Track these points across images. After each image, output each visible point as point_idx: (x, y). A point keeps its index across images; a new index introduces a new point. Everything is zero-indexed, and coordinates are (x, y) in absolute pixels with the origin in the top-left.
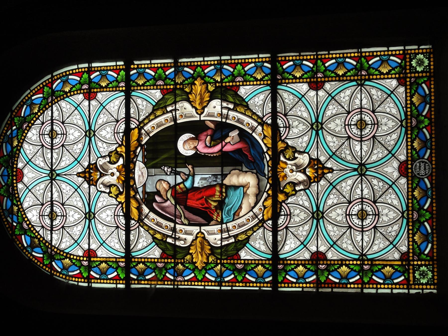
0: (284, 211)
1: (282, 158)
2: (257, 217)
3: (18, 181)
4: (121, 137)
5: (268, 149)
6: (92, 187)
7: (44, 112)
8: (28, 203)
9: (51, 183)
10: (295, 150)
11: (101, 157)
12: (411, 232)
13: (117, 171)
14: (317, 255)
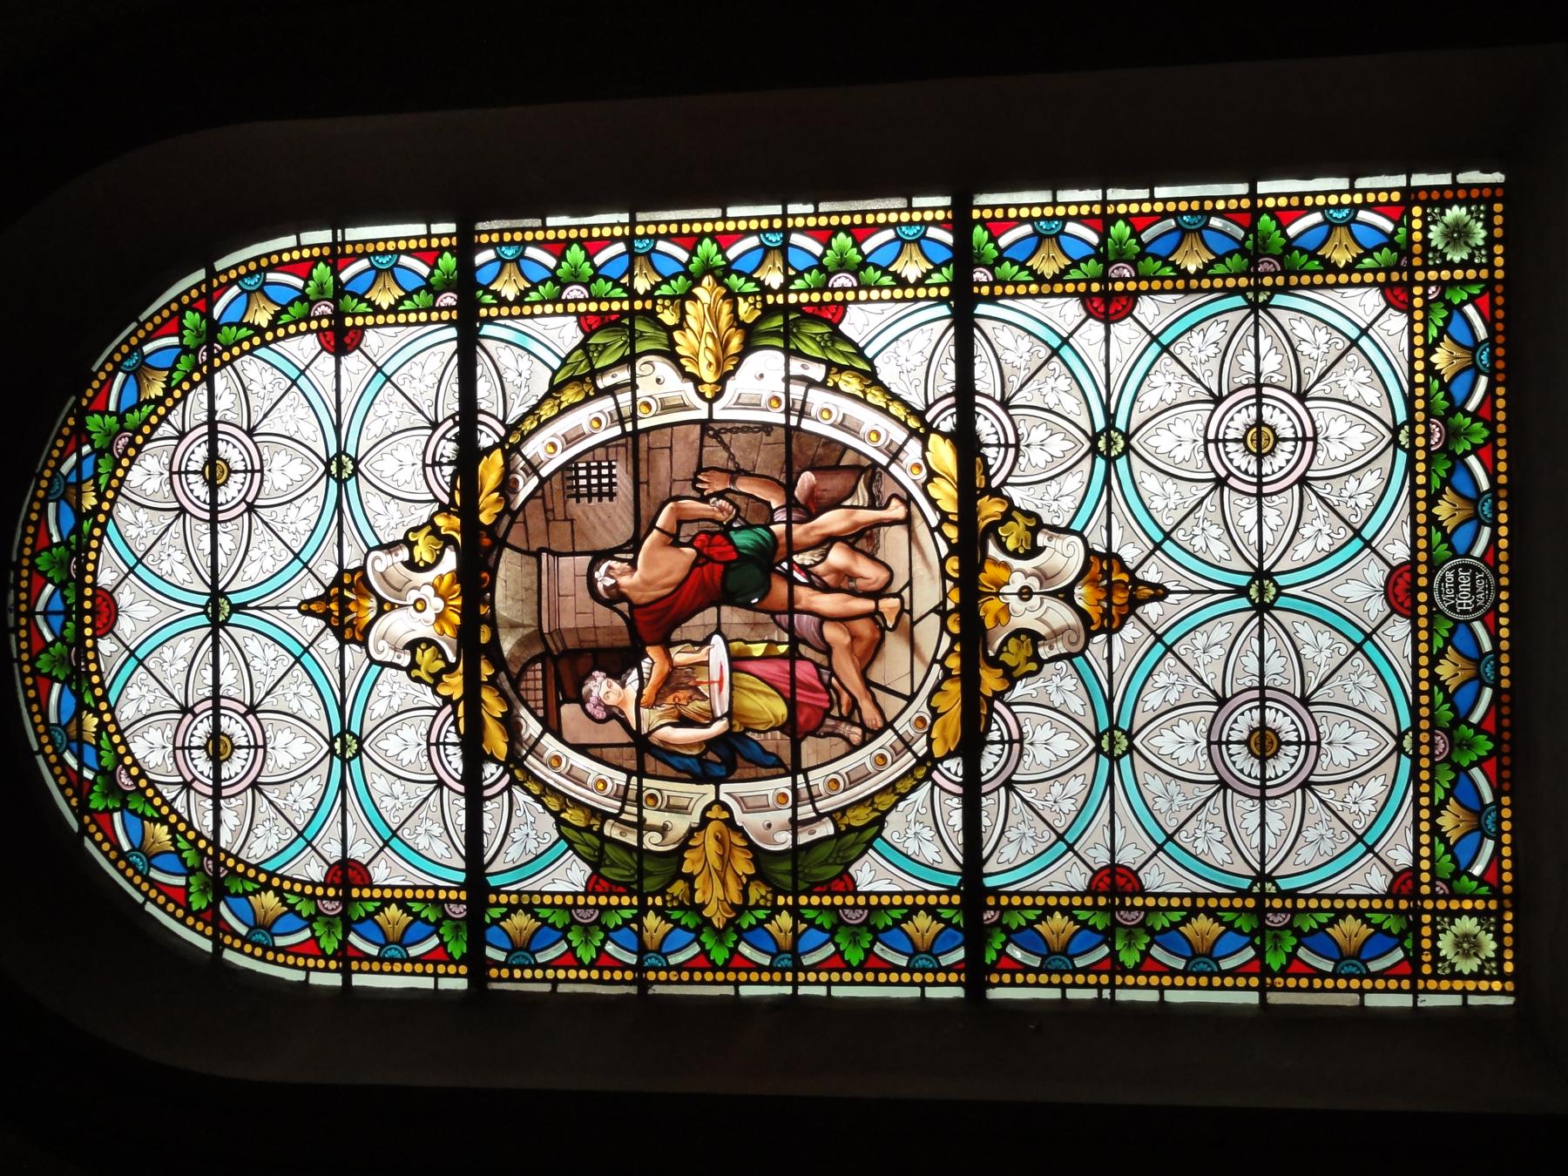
2: (908, 747)
6: (353, 654)
7: (185, 394)
10: (1036, 525)
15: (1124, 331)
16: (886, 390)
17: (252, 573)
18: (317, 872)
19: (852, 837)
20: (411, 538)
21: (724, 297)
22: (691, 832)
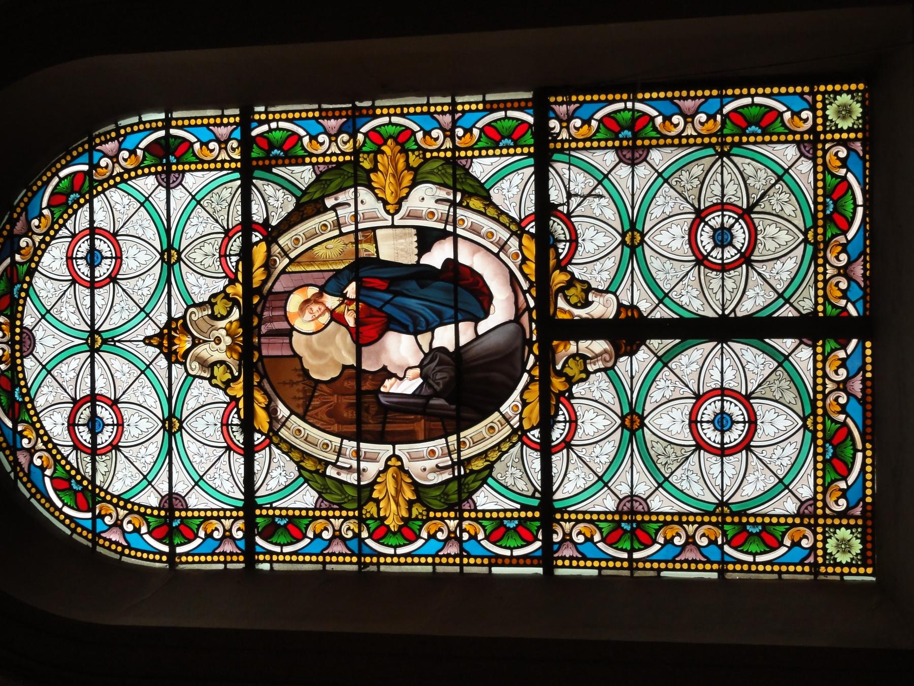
0: (564, 414)
1: (561, 303)
2: (508, 421)
3: (24, 354)
4: (234, 264)
5: (531, 284)
6: (177, 370)
7: (75, 212)
8: (44, 398)
9: (92, 357)
10: (588, 288)
11: (195, 305)
12: (820, 458)
13: (228, 335)
14: (632, 501)
15: (642, 170)
16: (496, 207)
17: (116, 320)
18: (154, 501)
19: (472, 477)
20: (213, 300)
21: (400, 152)
22: (380, 473)
